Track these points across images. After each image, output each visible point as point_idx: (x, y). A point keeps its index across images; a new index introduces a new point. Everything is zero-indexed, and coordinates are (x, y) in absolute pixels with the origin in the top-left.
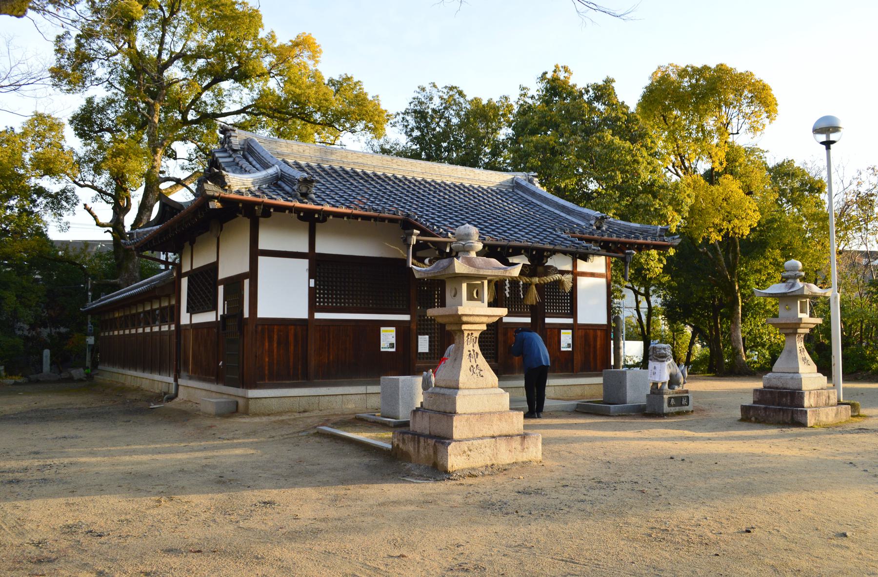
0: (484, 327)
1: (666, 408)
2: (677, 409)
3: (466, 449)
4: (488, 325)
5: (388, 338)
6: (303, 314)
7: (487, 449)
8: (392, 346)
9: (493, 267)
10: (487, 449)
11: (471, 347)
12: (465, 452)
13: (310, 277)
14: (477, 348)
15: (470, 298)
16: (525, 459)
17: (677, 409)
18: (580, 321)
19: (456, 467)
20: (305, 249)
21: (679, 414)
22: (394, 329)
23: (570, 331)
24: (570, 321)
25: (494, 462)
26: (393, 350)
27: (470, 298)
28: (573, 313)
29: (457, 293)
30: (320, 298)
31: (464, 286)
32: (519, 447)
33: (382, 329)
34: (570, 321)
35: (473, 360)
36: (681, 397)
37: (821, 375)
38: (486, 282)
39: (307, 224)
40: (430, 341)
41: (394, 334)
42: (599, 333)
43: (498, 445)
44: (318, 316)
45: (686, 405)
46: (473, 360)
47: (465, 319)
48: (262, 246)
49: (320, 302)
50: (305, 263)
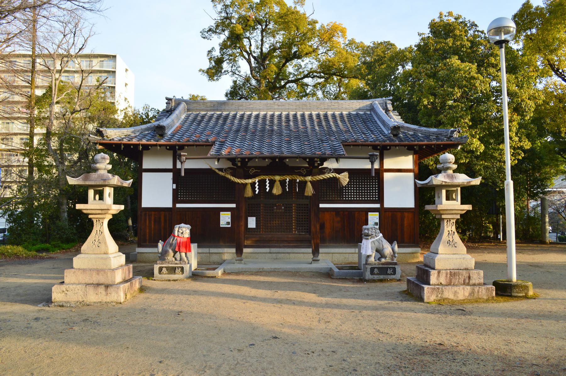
0: (458, 217)
1: (368, 276)
2: (382, 277)
3: (64, 290)
4: (461, 215)
5: (225, 219)
6: (170, 205)
7: (79, 291)
8: (228, 223)
9: (462, 179)
10: (79, 291)
11: (449, 229)
12: (63, 291)
13: (173, 183)
14: (454, 229)
15: (448, 199)
16: (108, 300)
17: (382, 277)
18: (386, 205)
19: (57, 300)
20: (170, 166)
21: (381, 281)
22: (230, 213)
23: (378, 213)
24: (378, 206)
25: (85, 300)
26: (230, 226)
27: (448, 199)
28: (381, 200)
29: (440, 197)
30: (181, 195)
31: (444, 192)
32: (104, 292)
33: (221, 213)
34: (378, 206)
35: (451, 237)
36: (388, 268)
37: (121, 254)
38: (459, 189)
39: (172, 152)
40: (256, 221)
41: (230, 216)
42: (406, 214)
43: (88, 290)
44: (178, 205)
45: (391, 274)
46: (451, 237)
47: (441, 212)
48: (144, 167)
49: (181, 197)
50: (170, 175)
